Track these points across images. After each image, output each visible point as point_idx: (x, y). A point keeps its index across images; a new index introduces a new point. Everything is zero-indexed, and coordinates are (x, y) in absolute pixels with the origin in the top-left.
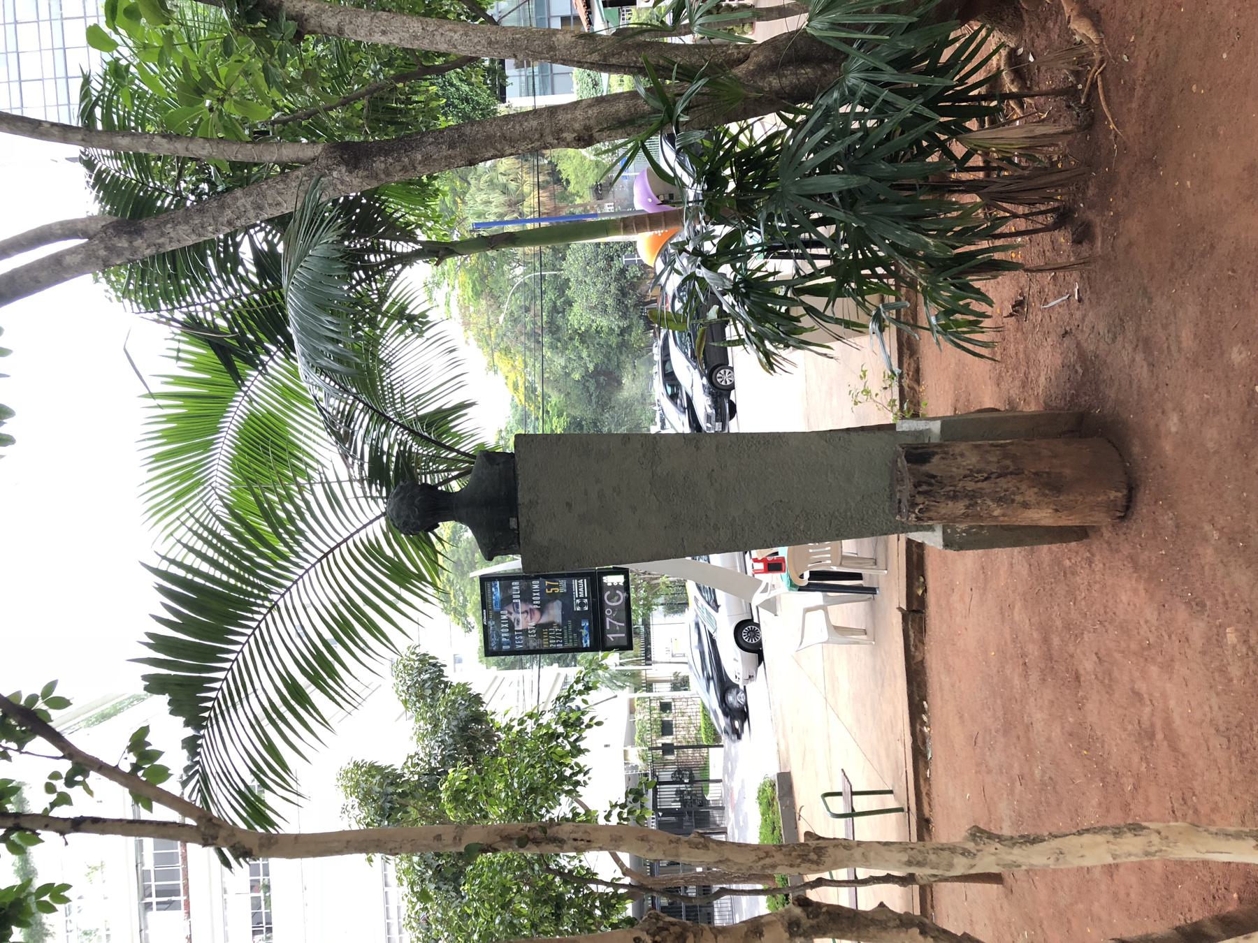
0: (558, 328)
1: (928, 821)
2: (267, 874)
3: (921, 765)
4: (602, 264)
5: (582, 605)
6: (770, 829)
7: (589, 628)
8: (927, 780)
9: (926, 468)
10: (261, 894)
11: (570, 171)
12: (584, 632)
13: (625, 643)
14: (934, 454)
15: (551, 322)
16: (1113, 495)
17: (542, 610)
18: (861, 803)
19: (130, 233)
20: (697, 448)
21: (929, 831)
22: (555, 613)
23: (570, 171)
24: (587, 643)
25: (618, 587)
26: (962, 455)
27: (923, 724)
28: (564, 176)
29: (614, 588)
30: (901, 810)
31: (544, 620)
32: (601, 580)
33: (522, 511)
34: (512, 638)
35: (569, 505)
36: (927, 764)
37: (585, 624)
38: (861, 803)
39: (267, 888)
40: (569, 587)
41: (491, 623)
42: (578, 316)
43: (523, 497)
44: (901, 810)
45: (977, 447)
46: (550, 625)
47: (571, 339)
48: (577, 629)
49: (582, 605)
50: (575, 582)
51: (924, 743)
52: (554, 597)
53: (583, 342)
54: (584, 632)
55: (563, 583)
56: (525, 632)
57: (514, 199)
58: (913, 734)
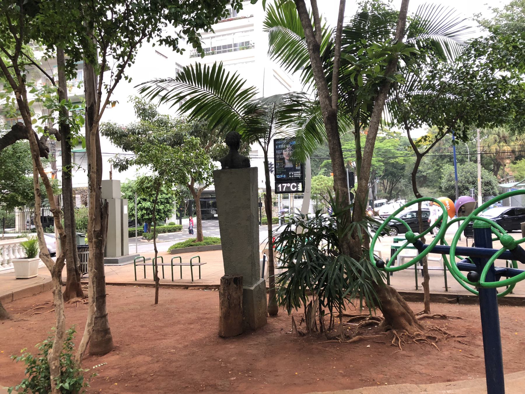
0: (443, 159)
1: (187, 288)
2: (218, 53)
3: (203, 287)
4: (471, 179)
5: (291, 175)
6: (215, 241)
7: (283, 178)
8: (199, 289)
9: (232, 283)
10: (211, 51)
11: (520, 165)
12: (282, 176)
13: (278, 191)
14: (237, 285)
15: (445, 156)
16: (223, 333)
17: (290, 160)
18: (196, 269)
19: (313, 49)
20: (247, 220)
21: (184, 289)
22: (289, 165)
23: (520, 165)
24: (278, 177)
25: (297, 189)
26: (236, 293)
27: (215, 289)
28: (518, 162)
29: (297, 187)
30: (193, 281)
31: (286, 161)
32: (300, 182)
33: (229, 170)
34: (280, 149)
35: (231, 183)
36: (203, 289)
37: (285, 176)
38: (196, 269)
39: (213, 54)
40: (298, 170)
41: (285, 141)
42: (448, 169)
43: (233, 170)
44: (193, 281)
45: (239, 298)
46: (284, 163)
47: (438, 165)
48: (283, 173)
49: (291, 175)
50: (299, 172)
51: (210, 289)
52: (294, 165)
53: (436, 170)
54: (282, 176)
55: (299, 168)
56: (282, 154)
57: (507, 139)
58: (212, 286)
